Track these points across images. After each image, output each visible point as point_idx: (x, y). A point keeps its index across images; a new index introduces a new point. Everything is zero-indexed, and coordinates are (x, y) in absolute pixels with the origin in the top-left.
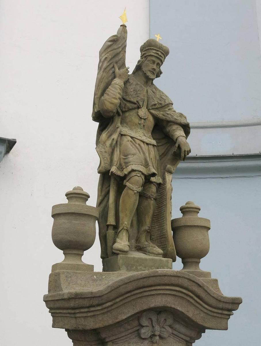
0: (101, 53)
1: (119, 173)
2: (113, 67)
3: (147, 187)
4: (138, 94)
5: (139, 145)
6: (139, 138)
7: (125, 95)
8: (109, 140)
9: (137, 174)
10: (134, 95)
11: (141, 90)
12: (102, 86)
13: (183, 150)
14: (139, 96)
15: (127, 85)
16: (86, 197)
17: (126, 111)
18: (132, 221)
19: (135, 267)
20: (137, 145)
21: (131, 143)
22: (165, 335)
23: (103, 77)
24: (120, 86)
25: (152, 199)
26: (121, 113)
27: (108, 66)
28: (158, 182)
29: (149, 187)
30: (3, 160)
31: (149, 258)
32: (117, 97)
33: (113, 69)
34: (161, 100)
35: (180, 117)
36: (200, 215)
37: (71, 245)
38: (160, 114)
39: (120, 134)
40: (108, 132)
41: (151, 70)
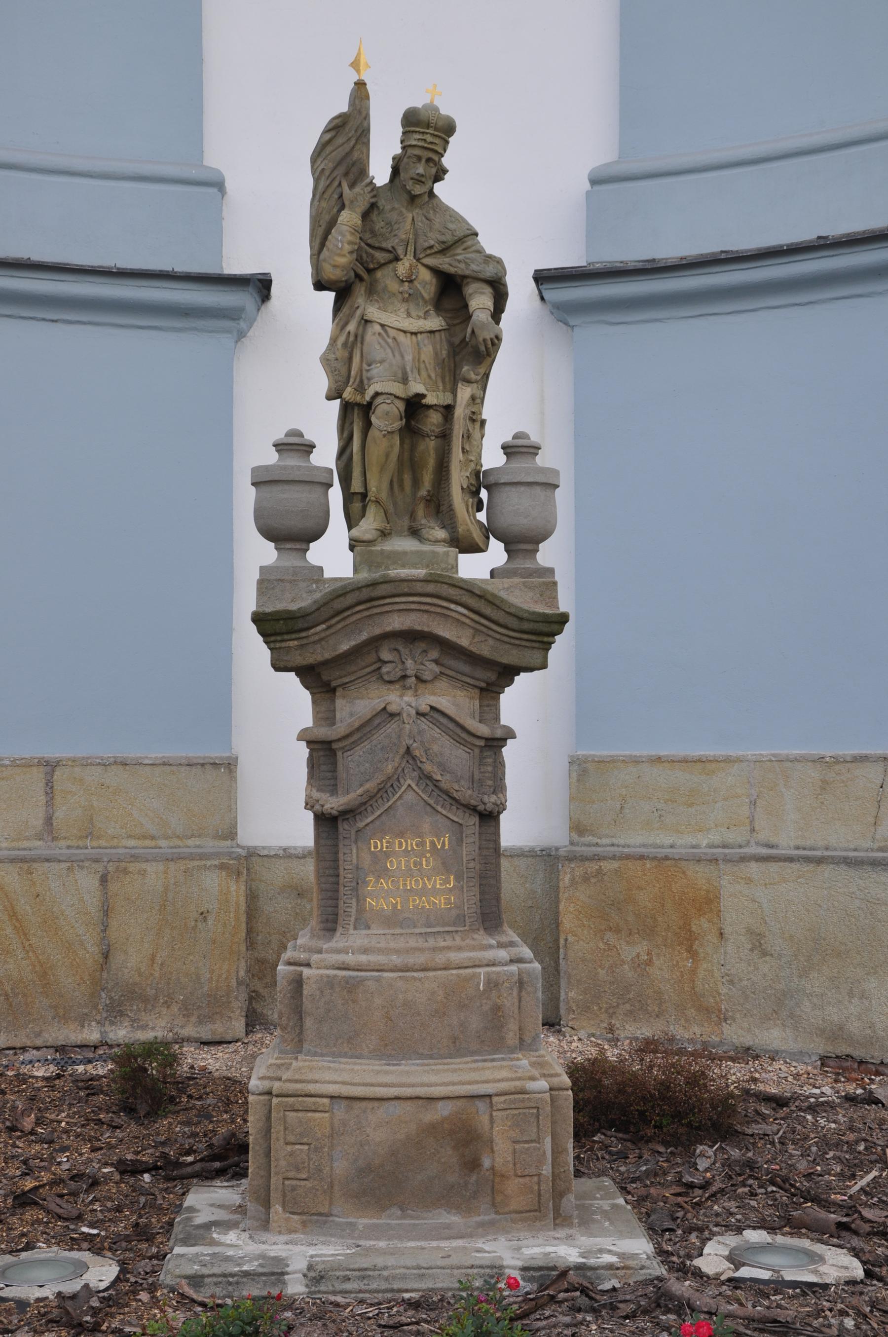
0: (314, 159)
1: (358, 399)
2: (340, 184)
5: (394, 338)
12: (320, 231)
13: (481, 339)
16: (308, 448)
17: (375, 269)
18: (392, 481)
20: (390, 341)
21: (381, 341)
22: (427, 676)
26: (365, 275)
27: (328, 186)
28: (446, 403)
30: (259, 318)
32: (345, 252)
36: (541, 460)
37: (293, 534)
38: (444, 263)
39: (362, 318)
41: (416, 177)
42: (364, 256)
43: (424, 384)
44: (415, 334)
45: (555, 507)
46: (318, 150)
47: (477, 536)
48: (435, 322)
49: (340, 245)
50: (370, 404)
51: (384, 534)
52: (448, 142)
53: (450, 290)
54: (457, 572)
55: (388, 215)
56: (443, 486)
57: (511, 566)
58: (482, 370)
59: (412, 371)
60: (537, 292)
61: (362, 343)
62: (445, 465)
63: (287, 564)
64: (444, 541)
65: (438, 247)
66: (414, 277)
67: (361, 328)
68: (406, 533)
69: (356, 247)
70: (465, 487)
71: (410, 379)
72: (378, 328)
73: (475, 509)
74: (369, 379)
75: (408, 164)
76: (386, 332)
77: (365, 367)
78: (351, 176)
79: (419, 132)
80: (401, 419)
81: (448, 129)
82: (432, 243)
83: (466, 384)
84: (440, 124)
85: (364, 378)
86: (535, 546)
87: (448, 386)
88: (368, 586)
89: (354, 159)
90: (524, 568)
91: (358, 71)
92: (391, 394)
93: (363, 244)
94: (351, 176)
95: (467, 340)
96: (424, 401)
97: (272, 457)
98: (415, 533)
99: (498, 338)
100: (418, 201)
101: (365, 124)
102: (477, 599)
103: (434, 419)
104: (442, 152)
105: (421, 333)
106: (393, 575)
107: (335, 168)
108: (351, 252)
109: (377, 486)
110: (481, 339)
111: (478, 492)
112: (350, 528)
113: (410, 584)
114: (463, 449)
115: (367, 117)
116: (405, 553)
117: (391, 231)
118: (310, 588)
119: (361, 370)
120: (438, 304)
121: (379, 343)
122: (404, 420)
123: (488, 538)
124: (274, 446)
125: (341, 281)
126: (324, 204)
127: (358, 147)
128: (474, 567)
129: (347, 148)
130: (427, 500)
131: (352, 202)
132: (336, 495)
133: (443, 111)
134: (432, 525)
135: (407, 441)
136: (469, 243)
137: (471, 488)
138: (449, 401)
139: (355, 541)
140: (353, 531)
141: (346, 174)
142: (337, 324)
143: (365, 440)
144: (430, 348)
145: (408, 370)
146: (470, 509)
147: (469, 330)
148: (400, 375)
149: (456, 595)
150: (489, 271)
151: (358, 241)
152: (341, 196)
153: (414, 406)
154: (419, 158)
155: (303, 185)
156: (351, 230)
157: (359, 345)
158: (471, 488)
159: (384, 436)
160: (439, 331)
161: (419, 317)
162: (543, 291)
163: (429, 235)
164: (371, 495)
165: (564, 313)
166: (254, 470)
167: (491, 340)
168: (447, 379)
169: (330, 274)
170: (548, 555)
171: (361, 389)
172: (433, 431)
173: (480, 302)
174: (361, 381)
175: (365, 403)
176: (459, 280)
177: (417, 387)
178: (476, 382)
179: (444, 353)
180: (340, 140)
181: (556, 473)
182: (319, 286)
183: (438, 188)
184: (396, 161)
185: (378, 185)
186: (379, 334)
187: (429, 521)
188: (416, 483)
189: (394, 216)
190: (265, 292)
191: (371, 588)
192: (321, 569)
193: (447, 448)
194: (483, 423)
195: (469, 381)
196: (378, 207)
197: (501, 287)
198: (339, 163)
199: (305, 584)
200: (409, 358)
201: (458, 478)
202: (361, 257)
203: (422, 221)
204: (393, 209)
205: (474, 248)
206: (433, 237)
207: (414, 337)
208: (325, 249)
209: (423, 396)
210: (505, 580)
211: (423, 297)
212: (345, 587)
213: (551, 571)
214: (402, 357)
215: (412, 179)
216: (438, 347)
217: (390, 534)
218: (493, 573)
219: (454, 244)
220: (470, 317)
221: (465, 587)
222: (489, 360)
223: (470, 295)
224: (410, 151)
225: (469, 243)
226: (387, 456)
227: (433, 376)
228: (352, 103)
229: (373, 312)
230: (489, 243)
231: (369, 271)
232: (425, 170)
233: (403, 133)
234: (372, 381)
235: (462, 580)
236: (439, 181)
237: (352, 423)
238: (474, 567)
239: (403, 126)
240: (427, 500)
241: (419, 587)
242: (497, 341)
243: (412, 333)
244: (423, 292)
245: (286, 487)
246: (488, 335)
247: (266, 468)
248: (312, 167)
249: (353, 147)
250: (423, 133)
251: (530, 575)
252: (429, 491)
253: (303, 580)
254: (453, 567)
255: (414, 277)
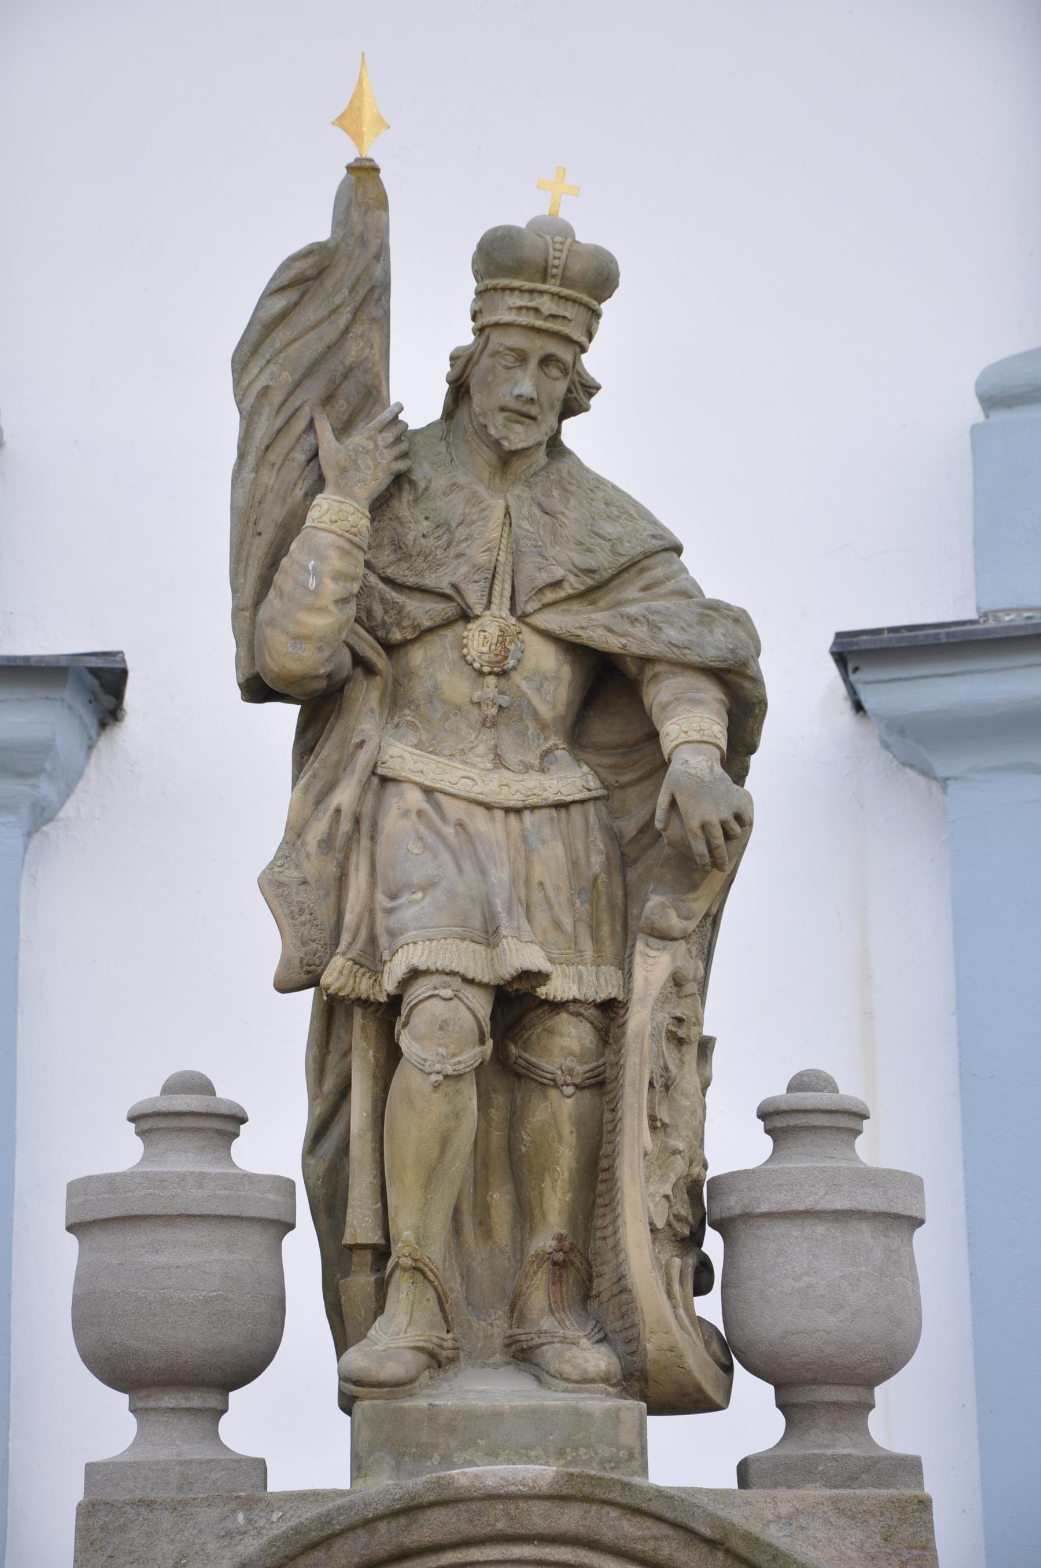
0: (241, 363)
1: (364, 987)
2: (311, 426)
3: (539, 1030)
4: (460, 542)
5: (461, 825)
6: (464, 787)
7: (393, 557)
8: (321, 815)
9: (435, 988)
10: (439, 552)
11: (475, 517)
12: (259, 548)
13: (695, 824)
14: (463, 555)
15: (400, 500)
17: (405, 643)
18: (457, 1211)
19: (436, 1458)
20: (449, 831)
21: (423, 830)
23: (257, 499)
24: (341, 536)
25: (564, 1088)
28: (603, 996)
29: (548, 1031)
30: (91, 771)
31: (512, 1407)
33: (311, 439)
34: (589, 550)
35: (700, 623)
36: (872, 1149)
37: (182, 1372)
38: (595, 626)
39: (374, 773)
40: (314, 776)
41: (513, 404)
42: (378, 610)
43: (543, 945)
44: (518, 811)
45: (915, 1280)
46: (254, 337)
47: (698, 1363)
48: (571, 780)
49: (312, 583)
50: (395, 1002)
51: (437, 1361)
52: (596, 315)
53: (607, 686)
54: (644, 1469)
55: (440, 503)
56: (599, 1222)
57: (797, 1450)
58: (699, 905)
59: (510, 912)
60: (842, 689)
61: (373, 838)
62: (604, 1163)
63: (166, 1454)
64: (606, 1380)
65: (574, 584)
66: (511, 662)
67: (370, 797)
68: (498, 1357)
69: (356, 587)
70: (660, 1224)
71: (504, 931)
72: (414, 798)
73: (690, 1288)
74: (392, 934)
75: (492, 370)
76: (437, 806)
77: (382, 900)
78: (342, 405)
79: (521, 291)
80: (482, 1041)
81: (601, 280)
82: (559, 573)
83: (661, 944)
84: (576, 268)
85: (380, 930)
86: (862, 1391)
87: (609, 949)
88: (393, 1514)
89: (349, 360)
90: (834, 1458)
91: (357, 137)
92: (452, 973)
93: (373, 579)
94: (342, 405)
95: (658, 825)
96: (542, 992)
97: (124, 1152)
98: (523, 1355)
99: (743, 820)
100: (519, 466)
101: (378, 272)
102: (705, 1549)
103: (568, 1042)
104: (583, 339)
105: (533, 808)
106: (463, 1481)
107: (297, 385)
108: (343, 601)
109: (418, 1224)
110: (695, 824)
111: (696, 1239)
112: (342, 1344)
113: (512, 1506)
114: (652, 1118)
115: (382, 253)
116: (496, 1416)
117: (449, 545)
118: (228, 1524)
119: (371, 911)
120: (577, 732)
121: (420, 838)
122: (490, 1043)
123: (729, 1369)
124: (132, 1119)
125: (316, 677)
126: (268, 478)
127: (358, 329)
128: (691, 1456)
129: (330, 333)
130: (555, 1263)
131: (343, 470)
132: (302, 1254)
133: (585, 236)
134: (570, 1333)
135: (499, 1100)
136: (659, 572)
137: (678, 1226)
138: (608, 988)
139: (357, 1383)
140: (352, 1354)
141: (328, 400)
142: (307, 789)
143: (386, 1089)
144: (557, 849)
145: (499, 905)
146: (676, 1287)
147: (663, 801)
148: (477, 922)
149: (644, 1539)
150: (714, 645)
151: (361, 570)
152: (315, 455)
153: (516, 1005)
154: (522, 357)
155: (212, 427)
156: (342, 542)
157: (365, 842)
158: (678, 1226)
159: (436, 1087)
160: (582, 802)
161: (527, 768)
162: (860, 688)
163: (550, 552)
164: (401, 1252)
165: (917, 746)
166: (75, 1189)
167: (724, 825)
168: (605, 930)
169: (289, 657)
170: (899, 1417)
171: (371, 960)
172: (570, 1072)
173: (689, 724)
174: (372, 940)
175: (383, 998)
176: (632, 668)
177: (522, 954)
178: (685, 937)
179: (597, 861)
180: (310, 314)
181: (913, 1184)
182: (258, 689)
183: (574, 432)
184: (460, 364)
185: (413, 426)
186: (420, 813)
187: (561, 1323)
188: (525, 1214)
189: (455, 507)
190: (109, 701)
191: (403, 1520)
192: (259, 1466)
193: (608, 1116)
194: (706, 1046)
195: (664, 936)
196: (412, 483)
197: (747, 684)
198: (309, 372)
199: (215, 1513)
200: (500, 875)
201: (640, 1203)
202: (369, 612)
203: (531, 517)
204: (454, 487)
205: (671, 585)
206: (563, 558)
207: (513, 818)
208: (272, 593)
209: (542, 977)
210: (781, 1492)
211: (536, 715)
212: (326, 1520)
213: (910, 1468)
214: (483, 872)
215: (503, 409)
216: (580, 846)
217: (452, 1360)
218: (744, 1470)
219: (619, 573)
220: (665, 765)
221: (668, 1514)
222: (717, 878)
223: (664, 707)
224: (498, 339)
225: (659, 572)
226: (445, 1142)
227: (567, 921)
228: (342, 217)
229: (403, 756)
230: (713, 571)
231: (390, 648)
232: (537, 386)
233: (479, 293)
234: (401, 940)
235: (660, 1493)
236: (574, 413)
237: (347, 1052)
238: (691, 1456)
239: (478, 275)
240: (555, 1263)
241: (537, 1517)
242: (736, 828)
243: (508, 810)
244: (536, 701)
245: (164, 1234)
246: (716, 813)
247: (111, 1182)
248: (237, 382)
249: (347, 330)
250: (531, 292)
251: (851, 1480)
252: (560, 1238)
253: (210, 1501)
254: (631, 1456)
255: (511, 662)
